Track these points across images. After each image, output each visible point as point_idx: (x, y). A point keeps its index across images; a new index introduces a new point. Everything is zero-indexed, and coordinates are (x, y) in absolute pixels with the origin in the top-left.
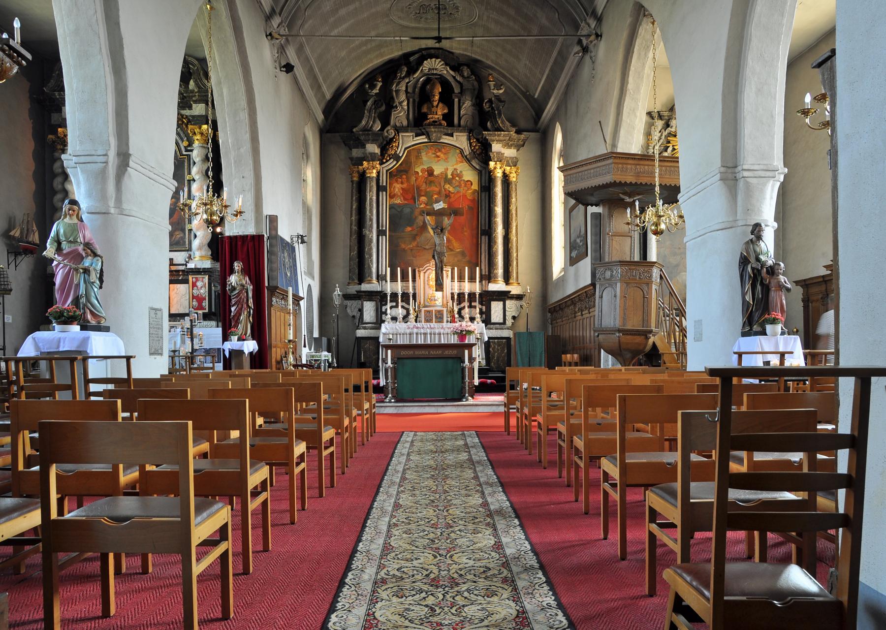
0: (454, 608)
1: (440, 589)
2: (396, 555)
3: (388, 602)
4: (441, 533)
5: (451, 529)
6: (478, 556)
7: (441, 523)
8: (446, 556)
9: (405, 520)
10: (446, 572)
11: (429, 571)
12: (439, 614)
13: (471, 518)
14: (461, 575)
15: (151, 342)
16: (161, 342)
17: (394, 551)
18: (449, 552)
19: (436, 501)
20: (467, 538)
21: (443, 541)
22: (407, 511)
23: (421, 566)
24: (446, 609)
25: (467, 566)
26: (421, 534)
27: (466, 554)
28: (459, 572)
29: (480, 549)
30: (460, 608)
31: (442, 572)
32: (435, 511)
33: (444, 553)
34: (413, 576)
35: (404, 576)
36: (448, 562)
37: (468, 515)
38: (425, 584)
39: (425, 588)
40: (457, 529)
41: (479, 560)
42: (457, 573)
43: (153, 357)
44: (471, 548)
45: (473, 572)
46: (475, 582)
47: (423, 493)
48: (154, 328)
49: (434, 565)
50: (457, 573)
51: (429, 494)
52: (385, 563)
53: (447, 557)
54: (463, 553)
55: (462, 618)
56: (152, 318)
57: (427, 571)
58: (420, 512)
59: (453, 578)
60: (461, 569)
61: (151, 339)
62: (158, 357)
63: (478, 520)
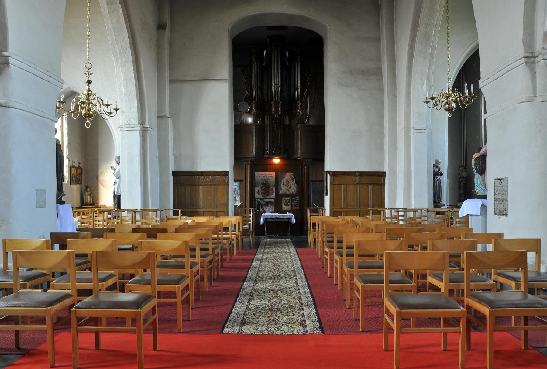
0: (269, 329)
1: (276, 307)
2: (295, 297)
3: (299, 332)
4: (275, 306)
5: (270, 308)
6: (256, 320)
7: (275, 311)
8: (272, 320)
9: (295, 313)
10: (273, 313)
11: (281, 314)
12: (276, 328)
13: (257, 314)
14: (267, 312)
15: (496, 205)
16: (505, 205)
17: (299, 323)
18: (270, 323)
19: (278, 302)
20: (258, 331)
21: (275, 302)
22: (293, 297)
23: (284, 316)
24: (273, 329)
25: (263, 316)
26: (285, 305)
27: (262, 321)
28: (268, 313)
29: (259, 298)
30: (267, 329)
31: (275, 313)
32: (279, 281)
33: (275, 297)
34: (288, 312)
35: (291, 312)
36: (272, 317)
37: (265, 280)
38: (282, 309)
39: (282, 308)
40: (267, 308)
41: (256, 318)
42: (268, 313)
43: (497, 216)
44: (263, 299)
45: (261, 313)
46: (262, 310)
47: (285, 289)
48: (499, 194)
49: (278, 316)
50: (268, 313)
51: (282, 289)
52: (301, 317)
53: (271, 320)
54: (263, 322)
55: (267, 326)
56: (497, 186)
57: (282, 314)
58: (286, 296)
59: (271, 311)
60: (267, 314)
61: (496, 202)
62: (503, 217)
63: (258, 292)
